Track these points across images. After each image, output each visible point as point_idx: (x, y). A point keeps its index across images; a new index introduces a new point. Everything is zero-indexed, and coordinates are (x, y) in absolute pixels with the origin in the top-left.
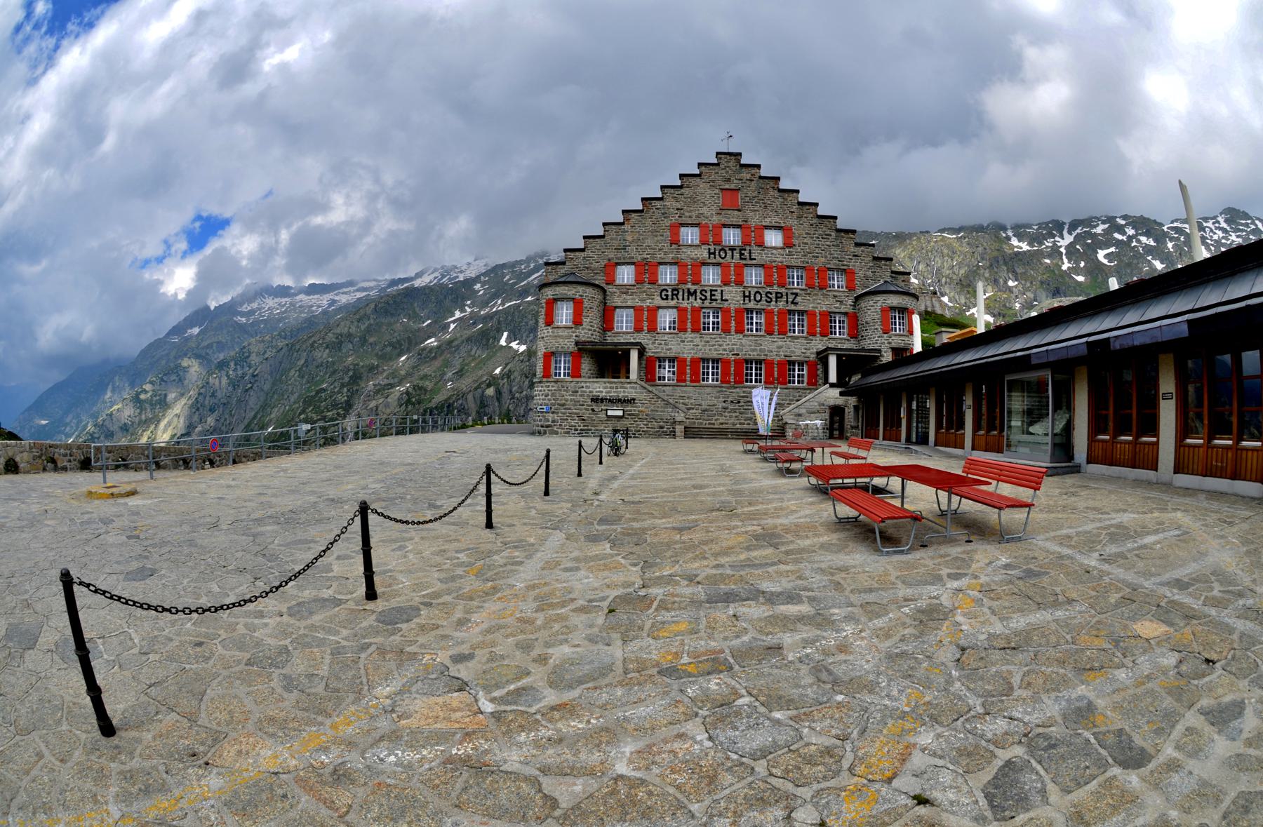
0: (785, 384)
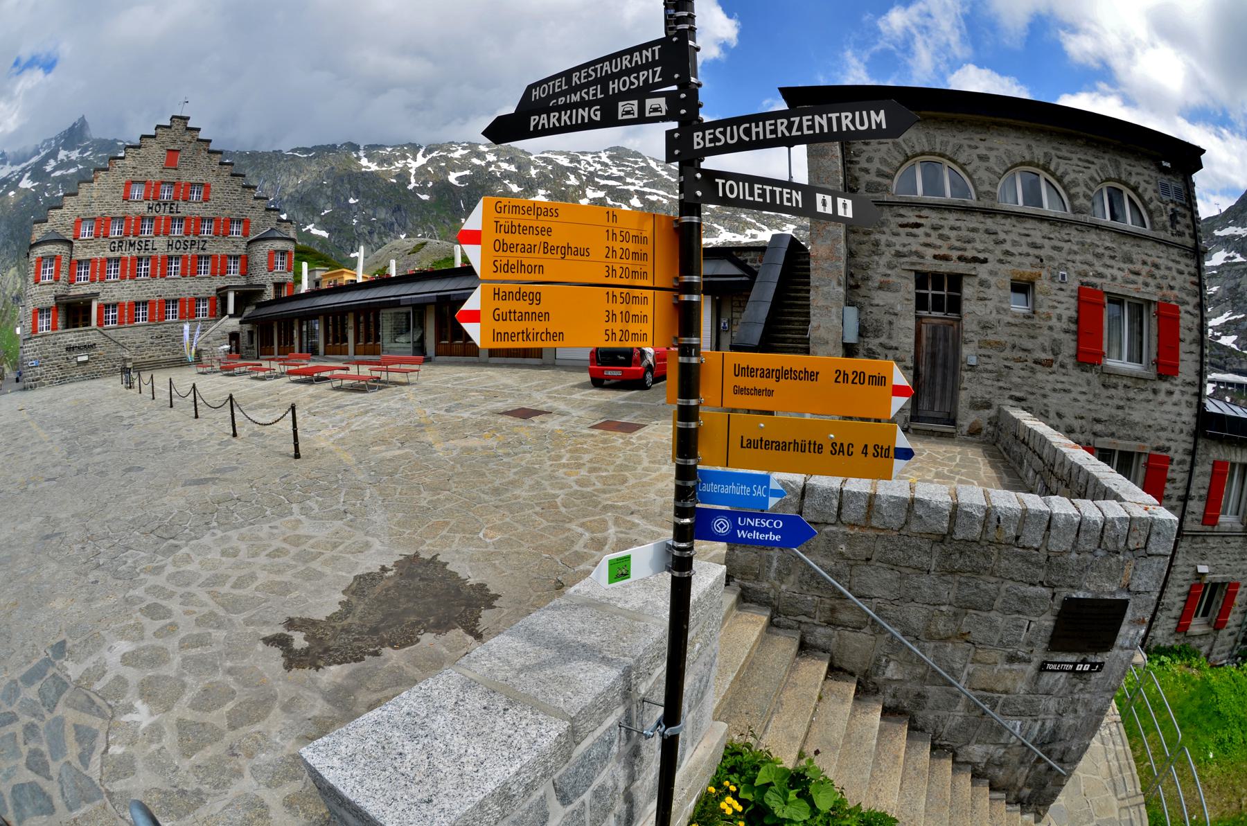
0: (193, 317)
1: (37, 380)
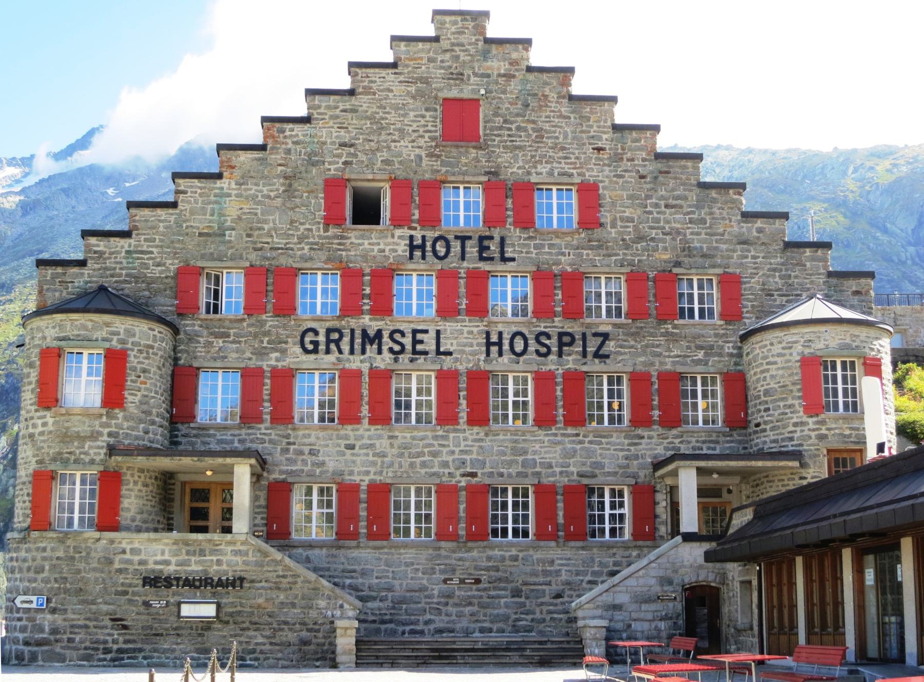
1: (39, 643)
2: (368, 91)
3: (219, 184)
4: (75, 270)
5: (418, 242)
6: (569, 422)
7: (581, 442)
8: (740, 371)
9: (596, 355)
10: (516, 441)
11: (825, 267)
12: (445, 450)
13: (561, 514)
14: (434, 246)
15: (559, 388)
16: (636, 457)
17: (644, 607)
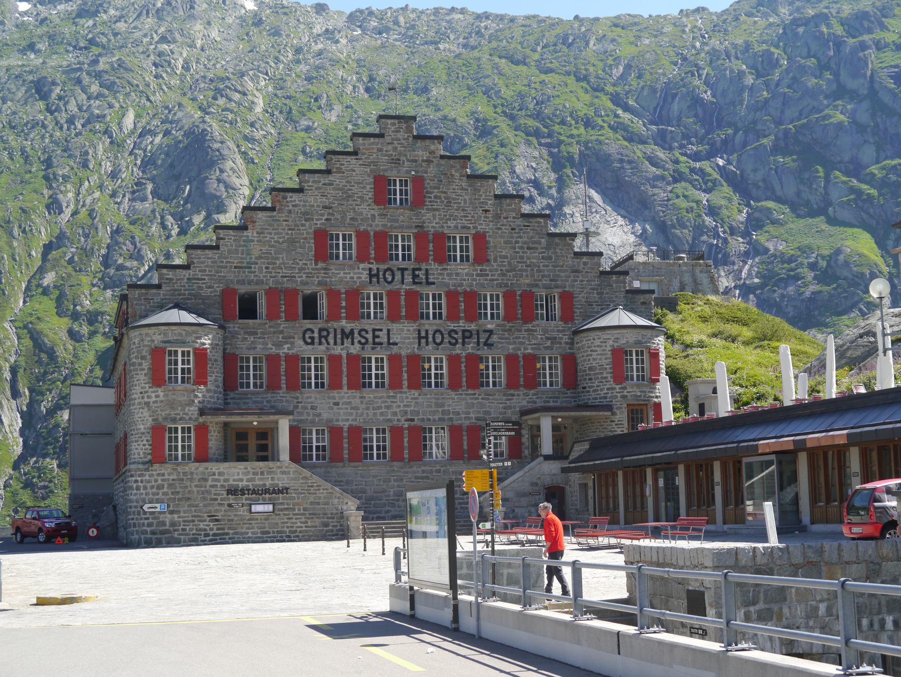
2: (339, 171)
3: (245, 233)
4: (154, 291)
5: (375, 272)
6: (469, 386)
7: (477, 399)
8: (573, 354)
9: (486, 344)
10: (438, 399)
11: (625, 287)
12: (394, 405)
13: (465, 443)
14: (384, 275)
15: (463, 365)
16: (510, 407)
17: (522, 499)
